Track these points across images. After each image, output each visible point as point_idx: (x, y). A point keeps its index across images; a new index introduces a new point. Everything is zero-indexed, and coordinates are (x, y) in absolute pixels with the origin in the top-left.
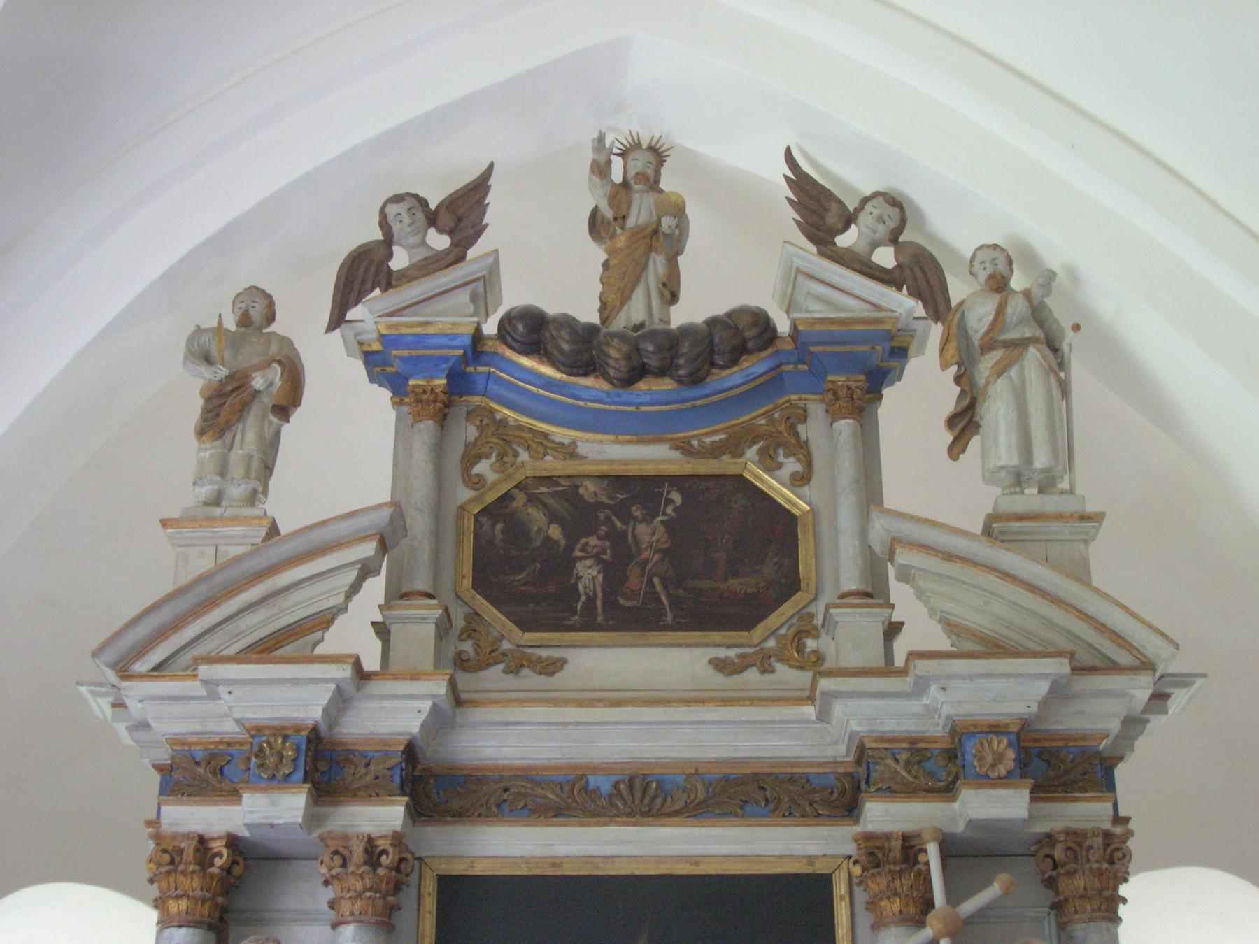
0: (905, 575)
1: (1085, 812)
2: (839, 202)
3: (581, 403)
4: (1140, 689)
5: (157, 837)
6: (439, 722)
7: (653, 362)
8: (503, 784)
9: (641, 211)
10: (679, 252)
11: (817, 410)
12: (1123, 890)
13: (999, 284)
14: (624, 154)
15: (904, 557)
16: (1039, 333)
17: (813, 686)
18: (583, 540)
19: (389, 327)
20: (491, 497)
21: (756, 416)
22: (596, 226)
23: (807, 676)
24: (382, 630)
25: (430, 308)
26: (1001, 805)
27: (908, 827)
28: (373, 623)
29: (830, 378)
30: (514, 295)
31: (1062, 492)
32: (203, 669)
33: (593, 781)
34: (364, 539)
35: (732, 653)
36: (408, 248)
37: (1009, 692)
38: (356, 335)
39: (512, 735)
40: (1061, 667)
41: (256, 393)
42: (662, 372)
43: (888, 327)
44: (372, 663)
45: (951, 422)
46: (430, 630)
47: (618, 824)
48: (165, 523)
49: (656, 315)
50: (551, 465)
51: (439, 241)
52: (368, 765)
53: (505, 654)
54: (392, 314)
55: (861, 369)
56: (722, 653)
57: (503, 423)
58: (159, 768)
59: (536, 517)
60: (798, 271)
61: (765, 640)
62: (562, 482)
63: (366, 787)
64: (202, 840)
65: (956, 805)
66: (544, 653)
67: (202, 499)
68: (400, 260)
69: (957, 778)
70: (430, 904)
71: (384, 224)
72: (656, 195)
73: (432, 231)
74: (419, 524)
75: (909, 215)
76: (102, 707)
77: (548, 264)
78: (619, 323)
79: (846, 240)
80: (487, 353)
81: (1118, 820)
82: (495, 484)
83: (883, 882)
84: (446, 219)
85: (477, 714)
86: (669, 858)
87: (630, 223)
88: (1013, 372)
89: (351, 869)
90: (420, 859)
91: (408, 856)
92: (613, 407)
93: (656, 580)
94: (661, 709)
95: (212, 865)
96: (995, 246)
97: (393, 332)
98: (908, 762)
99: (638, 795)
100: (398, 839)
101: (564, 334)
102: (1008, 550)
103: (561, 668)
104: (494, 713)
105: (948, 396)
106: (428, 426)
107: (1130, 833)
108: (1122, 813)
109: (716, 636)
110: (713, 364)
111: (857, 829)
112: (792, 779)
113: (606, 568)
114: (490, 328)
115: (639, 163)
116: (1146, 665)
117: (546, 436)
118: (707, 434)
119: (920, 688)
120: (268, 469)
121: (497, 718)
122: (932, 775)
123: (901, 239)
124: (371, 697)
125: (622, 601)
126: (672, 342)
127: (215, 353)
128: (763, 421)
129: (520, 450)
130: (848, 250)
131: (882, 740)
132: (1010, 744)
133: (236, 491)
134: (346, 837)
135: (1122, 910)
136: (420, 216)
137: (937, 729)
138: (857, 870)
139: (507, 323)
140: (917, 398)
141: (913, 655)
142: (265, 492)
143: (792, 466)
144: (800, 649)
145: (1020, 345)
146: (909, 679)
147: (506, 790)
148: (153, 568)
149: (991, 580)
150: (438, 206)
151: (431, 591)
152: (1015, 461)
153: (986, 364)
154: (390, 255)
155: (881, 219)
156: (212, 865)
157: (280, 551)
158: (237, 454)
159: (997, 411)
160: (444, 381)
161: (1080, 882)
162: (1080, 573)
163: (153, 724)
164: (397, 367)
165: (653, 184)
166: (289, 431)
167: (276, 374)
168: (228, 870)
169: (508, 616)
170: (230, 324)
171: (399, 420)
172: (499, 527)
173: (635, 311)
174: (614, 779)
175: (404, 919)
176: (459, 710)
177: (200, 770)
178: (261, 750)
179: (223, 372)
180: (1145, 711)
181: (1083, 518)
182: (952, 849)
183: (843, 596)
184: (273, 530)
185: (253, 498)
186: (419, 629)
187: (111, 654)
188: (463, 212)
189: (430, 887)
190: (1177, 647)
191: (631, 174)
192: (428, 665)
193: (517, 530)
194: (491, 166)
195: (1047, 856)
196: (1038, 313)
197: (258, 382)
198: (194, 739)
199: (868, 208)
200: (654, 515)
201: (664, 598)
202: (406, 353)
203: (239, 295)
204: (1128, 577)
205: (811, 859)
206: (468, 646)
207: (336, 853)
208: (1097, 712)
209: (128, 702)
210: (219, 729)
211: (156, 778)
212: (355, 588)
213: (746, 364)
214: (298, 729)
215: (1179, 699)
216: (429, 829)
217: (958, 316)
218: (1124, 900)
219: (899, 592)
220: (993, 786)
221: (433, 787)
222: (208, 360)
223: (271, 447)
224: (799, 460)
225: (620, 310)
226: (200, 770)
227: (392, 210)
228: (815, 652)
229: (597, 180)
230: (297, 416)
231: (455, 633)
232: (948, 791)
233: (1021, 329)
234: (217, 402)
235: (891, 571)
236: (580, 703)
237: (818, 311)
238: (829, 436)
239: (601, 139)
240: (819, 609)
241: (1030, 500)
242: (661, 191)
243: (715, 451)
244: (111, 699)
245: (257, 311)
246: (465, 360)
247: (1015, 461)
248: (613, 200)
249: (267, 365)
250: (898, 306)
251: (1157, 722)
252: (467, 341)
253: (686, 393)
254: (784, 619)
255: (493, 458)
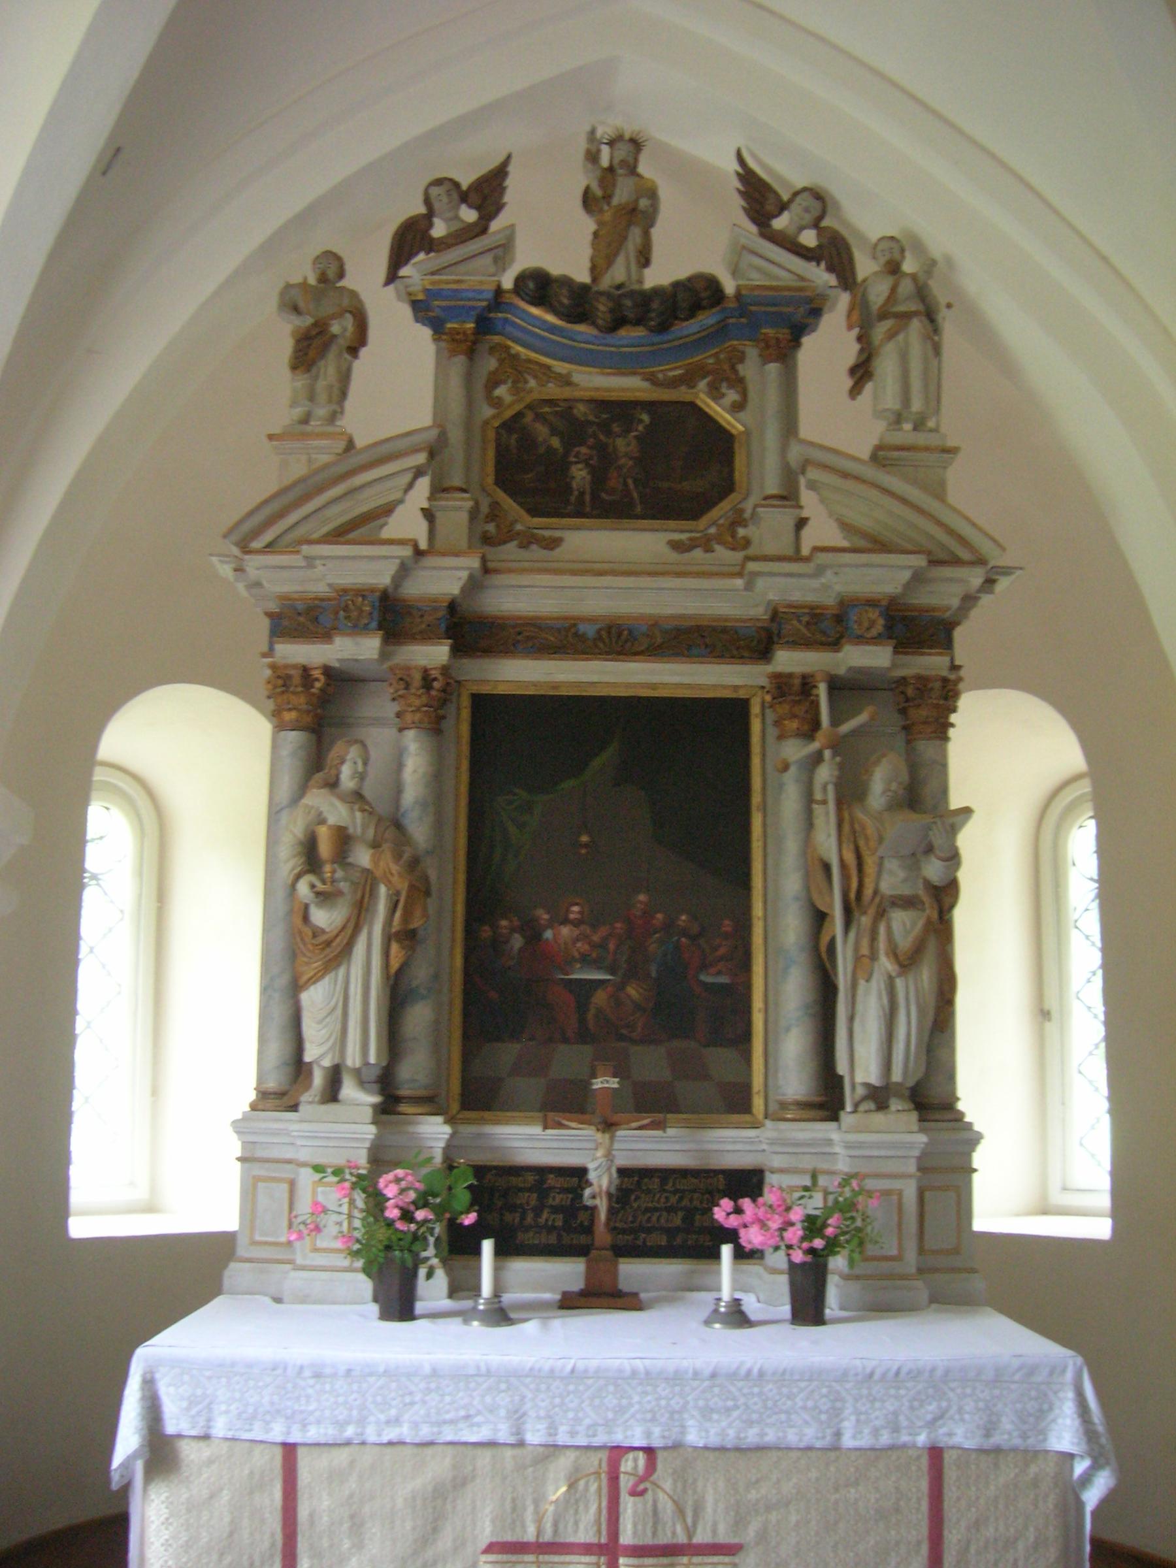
0: (812, 486)
1: (931, 663)
2: (775, 193)
3: (576, 344)
4: (975, 578)
5: (273, 667)
6: (474, 585)
7: (630, 315)
8: (518, 629)
9: (623, 193)
10: (652, 225)
11: (752, 353)
12: (953, 718)
13: (893, 268)
14: (611, 143)
15: (813, 474)
16: (921, 307)
17: (743, 566)
18: (577, 449)
19: (433, 283)
20: (508, 414)
21: (707, 356)
22: (589, 201)
23: (739, 556)
24: (428, 515)
25: (462, 268)
26: (876, 657)
27: (806, 669)
28: (422, 509)
29: (764, 331)
30: (524, 259)
31: (931, 431)
32: (306, 549)
33: (582, 628)
34: (416, 450)
35: (684, 537)
36: (446, 220)
37: (885, 578)
38: (406, 287)
39: (523, 595)
40: (920, 561)
41: (334, 336)
42: (639, 322)
43: (808, 294)
44: (423, 545)
45: (853, 371)
46: (464, 517)
47: (599, 659)
48: (271, 437)
49: (634, 276)
50: (553, 390)
51: (469, 215)
52: (422, 616)
53: (518, 534)
54: (433, 274)
55: (784, 324)
56: (677, 536)
57: (516, 357)
58: (269, 615)
59: (541, 431)
60: (744, 248)
61: (709, 527)
62: (562, 404)
63: (421, 632)
64: (305, 670)
65: (840, 655)
66: (547, 533)
67: (295, 418)
68: (439, 230)
69: (842, 637)
70: (466, 714)
71: (427, 202)
72: (637, 179)
73: (464, 207)
74: (456, 435)
75: (830, 210)
76: (226, 570)
77: (550, 235)
78: (606, 283)
79: (779, 223)
80: (506, 303)
81: (955, 668)
82: (509, 406)
83: (787, 707)
84: (474, 198)
85: (497, 579)
86: (635, 685)
87: (615, 201)
88: (900, 337)
89: (413, 691)
90: (459, 682)
91: (451, 681)
92: (600, 348)
93: (630, 481)
94: (632, 579)
95: (312, 687)
96: (892, 238)
97: (437, 287)
98: (808, 623)
99: (614, 640)
100: (445, 670)
101: (565, 291)
102: (888, 473)
103: (558, 546)
104: (514, 579)
105: (850, 352)
106: (460, 361)
107: (960, 679)
108: (957, 663)
109: (672, 524)
110: (676, 318)
111: (769, 669)
112: (725, 630)
113: (593, 471)
114: (508, 283)
115: (622, 151)
116: (981, 561)
117: (548, 368)
118: (671, 370)
119: (820, 571)
120: (344, 394)
121: (514, 582)
122: (824, 633)
123: (824, 224)
124: (425, 568)
125: (604, 495)
126: (645, 299)
127: (301, 305)
128: (711, 361)
129: (529, 378)
130: (781, 233)
131: (790, 606)
132: (881, 614)
133: (322, 412)
134: (408, 668)
135: (952, 732)
136: (455, 196)
137: (829, 600)
138: (768, 698)
139: (520, 280)
140: (827, 349)
141: (816, 549)
142: (342, 413)
143: (732, 396)
144: (733, 536)
145: (906, 317)
146: (812, 565)
147: (519, 634)
148: (265, 475)
149: (874, 494)
150: (470, 188)
151: (464, 487)
152: (897, 406)
153: (880, 330)
154: (431, 225)
155: (807, 210)
156: (312, 687)
157: (353, 458)
158: (321, 384)
159: (887, 366)
160: (471, 325)
161: (923, 713)
162: (939, 492)
163: (265, 583)
164: (437, 312)
165: (633, 171)
166: (357, 366)
167: (349, 322)
168: (322, 690)
169: (520, 504)
170: (312, 281)
171: (438, 352)
172: (515, 436)
173: (618, 273)
174: (598, 627)
175: (448, 725)
176: (488, 576)
177: (299, 619)
178: (347, 606)
179: (309, 321)
180: (979, 591)
181: (946, 450)
182: (837, 686)
183: (766, 498)
184: (350, 445)
185: (333, 418)
186: (456, 515)
187: (235, 537)
188: (488, 193)
189: (466, 702)
190: (1003, 549)
191: (616, 162)
192: (464, 543)
193: (528, 441)
194: (509, 157)
195: (902, 693)
196: (922, 293)
197: (335, 328)
198: (296, 596)
199: (798, 199)
200: (629, 431)
201: (635, 495)
202: (444, 303)
203: (318, 257)
204: (974, 494)
205: (736, 688)
206: (491, 528)
207: (401, 679)
208: (942, 594)
209: (248, 569)
210: (315, 590)
211: (266, 623)
212: (410, 486)
213: (700, 317)
214: (372, 591)
215: (1003, 584)
216: (465, 661)
217: (862, 290)
218: (952, 725)
219: (807, 497)
220: (867, 643)
221: (469, 630)
222: (296, 309)
223: (345, 378)
224: (738, 392)
225: (606, 272)
226: (301, 619)
227: (434, 191)
228: (744, 538)
229: (590, 166)
230: (363, 352)
231: (482, 516)
232: (834, 645)
233: (909, 306)
234: (305, 344)
235: (802, 481)
236: (574, 573)
237: (757, 280)
238: (760, 374)
239: (593, 132)
240: (748, 506)
241: (906, 434)
242: (639, 176)
243: (674, 383)
244: (233, 565)
245: (331, 270)
246: (489, 309)
247: (897, 406)
248: (602, 182)
249: (340, 315)
250: (814, 273)
251: (986, 599)
252: (490, 295)
253: (656, 339)
254: (722, 513)
255: (509, 384)
